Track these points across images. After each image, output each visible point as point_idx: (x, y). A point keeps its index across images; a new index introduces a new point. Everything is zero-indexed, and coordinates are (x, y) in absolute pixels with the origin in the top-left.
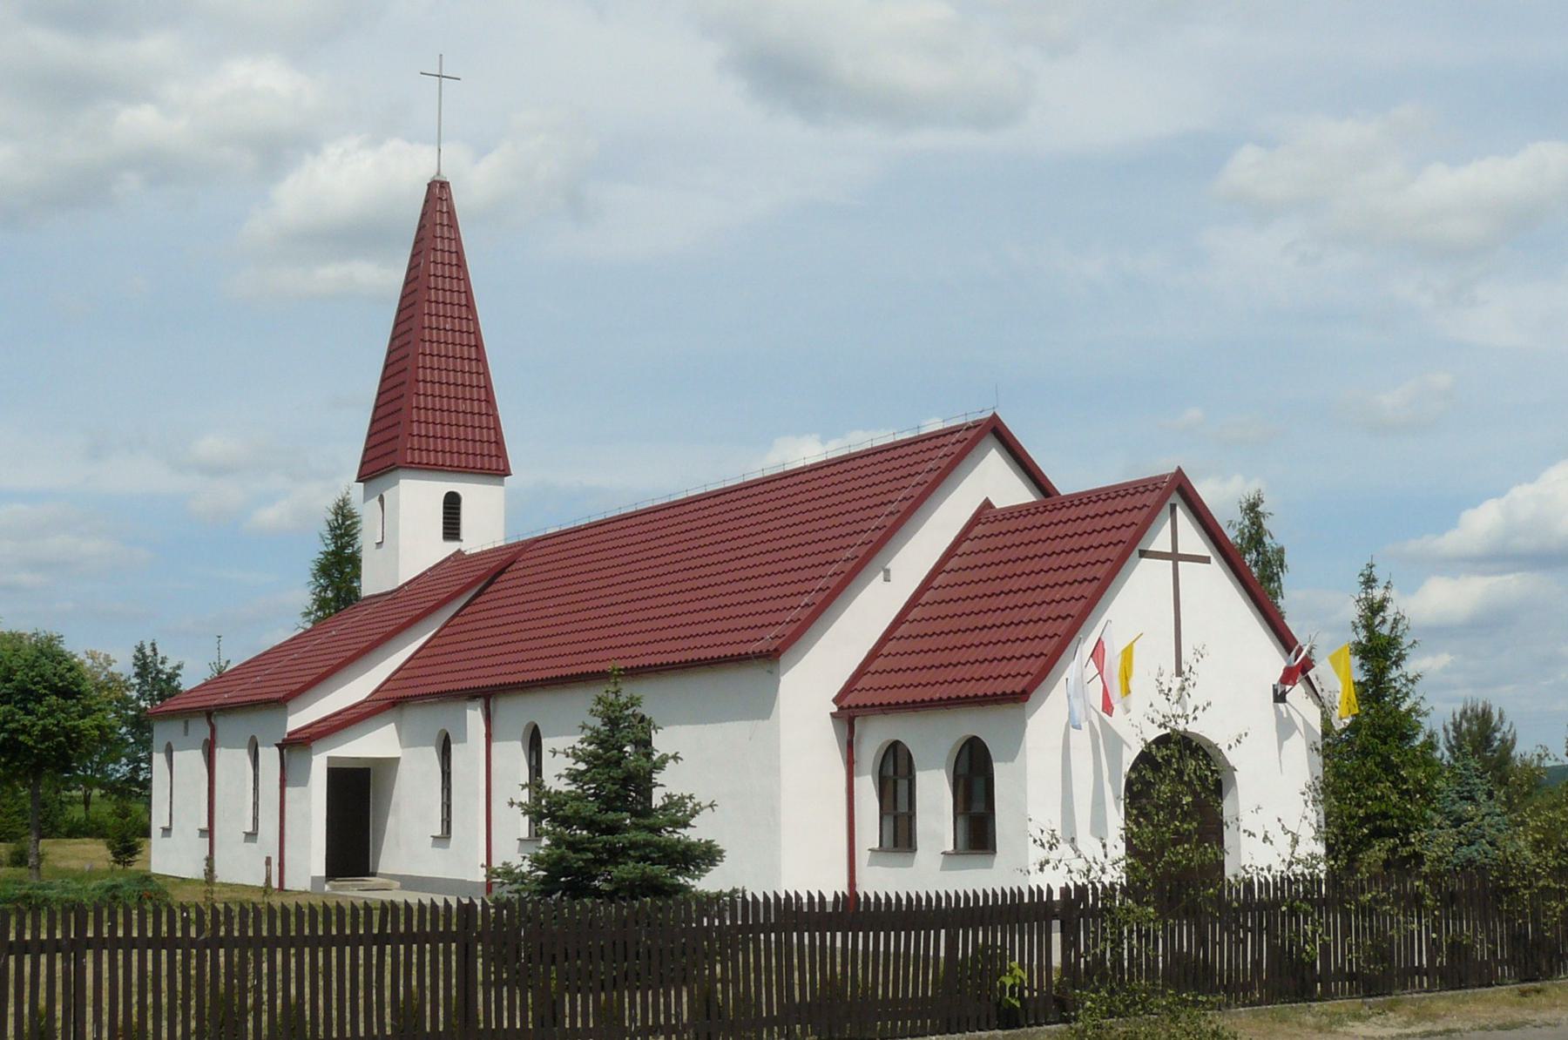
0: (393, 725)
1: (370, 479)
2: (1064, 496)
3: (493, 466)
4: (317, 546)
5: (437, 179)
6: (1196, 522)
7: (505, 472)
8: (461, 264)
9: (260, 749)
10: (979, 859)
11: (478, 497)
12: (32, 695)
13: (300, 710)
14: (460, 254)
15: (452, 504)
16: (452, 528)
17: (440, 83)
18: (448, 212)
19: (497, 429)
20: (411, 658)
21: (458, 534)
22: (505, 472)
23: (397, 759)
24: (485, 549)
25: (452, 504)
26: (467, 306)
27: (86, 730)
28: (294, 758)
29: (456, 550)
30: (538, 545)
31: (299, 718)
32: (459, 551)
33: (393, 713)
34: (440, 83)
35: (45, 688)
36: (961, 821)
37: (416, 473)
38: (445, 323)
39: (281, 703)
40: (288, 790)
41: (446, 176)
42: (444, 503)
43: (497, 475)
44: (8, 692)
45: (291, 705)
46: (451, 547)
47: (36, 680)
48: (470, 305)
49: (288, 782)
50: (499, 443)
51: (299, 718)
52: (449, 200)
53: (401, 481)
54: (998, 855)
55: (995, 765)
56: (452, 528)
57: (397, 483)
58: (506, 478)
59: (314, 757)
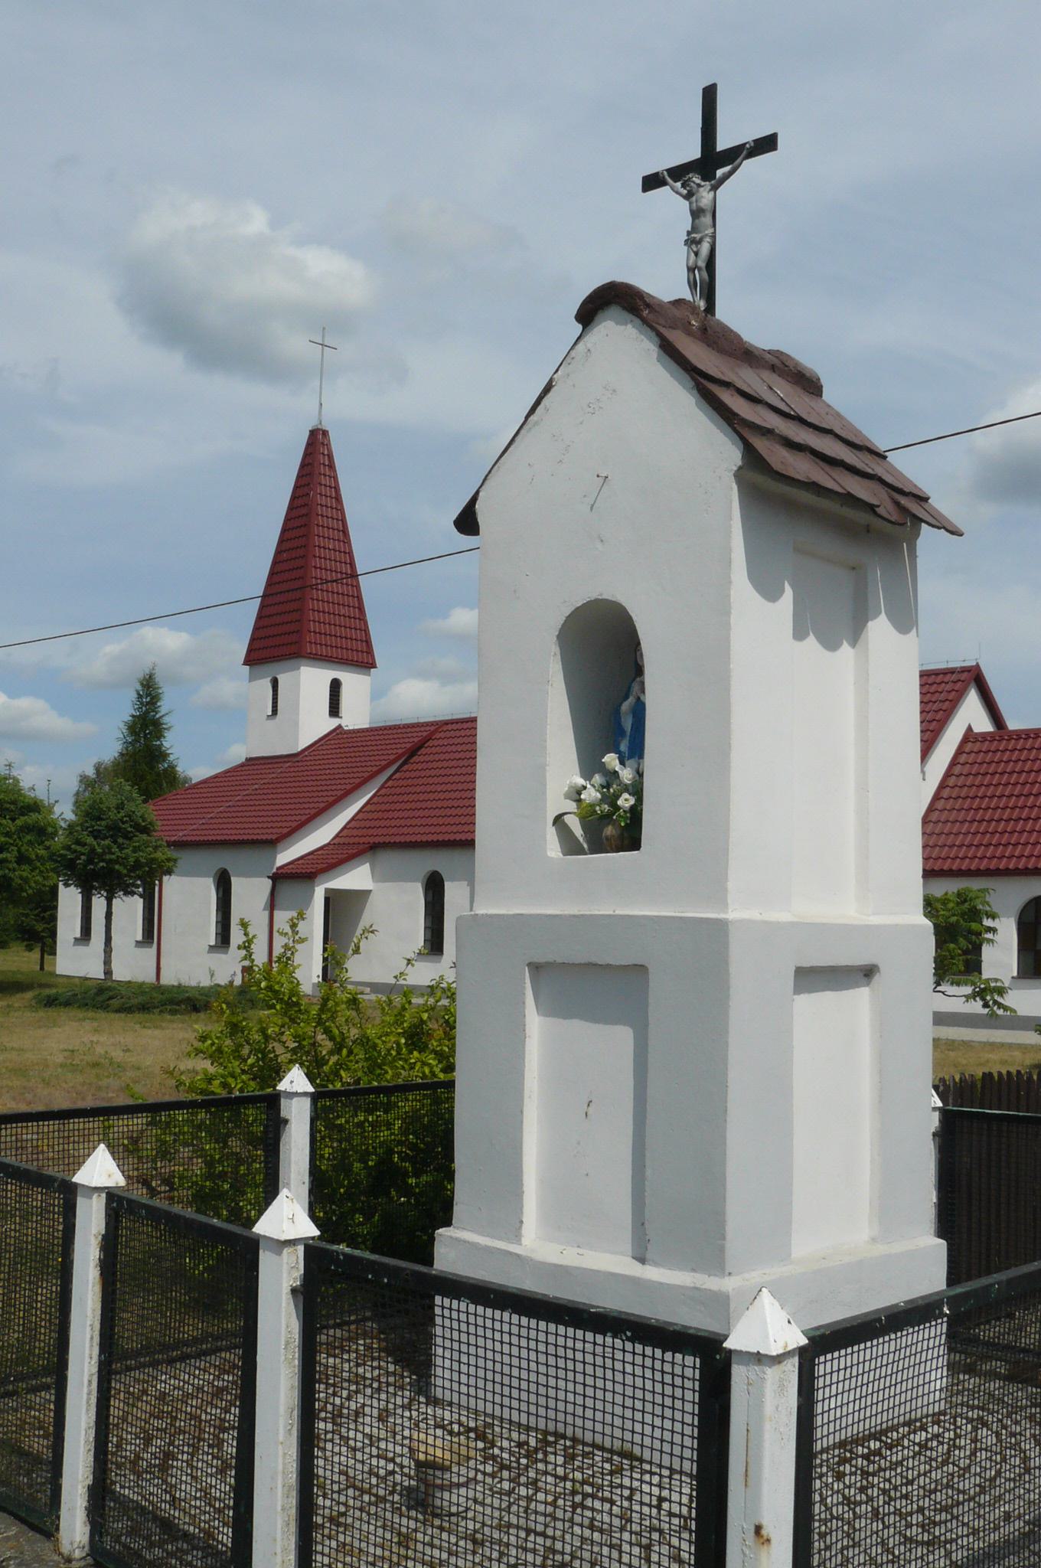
0: (368, 864)
1: (256, 664)
2: (976, 734)
3: (364, 661)
4: (125, 708)
5: (319, 427)
6: (320, 663)
7: (373, 665)
8: (338, 499)
9: (235, 881)
10: (435, 957)
11: (353, 683)
12: (120, 832)
13: (286, 849)
14: (337, 489)
15: (335, 686)
16: (334, 710)
17: (323, 349)
18: (328, 455)
19: (366, 631)
20: (360, 811)
21: (338, 712)
22: (373, 665)
23: (366, 894)
24: (356, 727)
25: (335, 686)
26: (344, 532)
27: (163, 861)
28: (287, 890)
29: (337, 724)
30: (450, 727)
31: (287, 855)
32: (340, 727)
33: (368, 855)
34: (323, 349)
35: (131, 826)
36: (220, 913)
37: (353, 668)
38: (329, 543)
39: (273, 843)
40: (276, 913)
41: (326, 426)
42: (331, 687)
43: (365, 667)
44: (100, 828)
45: (280, 846)
46: (334, 723)
47: (125, 819)
48: (345, 532)
49: (276, 907)
50: (368, 642)
51: (287, 855)
52: (328, 445)
53: (302, 668)
54: (445, 956)
55: (446, 884)
56: (334, 710)
57: (299, 669)
58: (372, 670)
59: (316, 888)
